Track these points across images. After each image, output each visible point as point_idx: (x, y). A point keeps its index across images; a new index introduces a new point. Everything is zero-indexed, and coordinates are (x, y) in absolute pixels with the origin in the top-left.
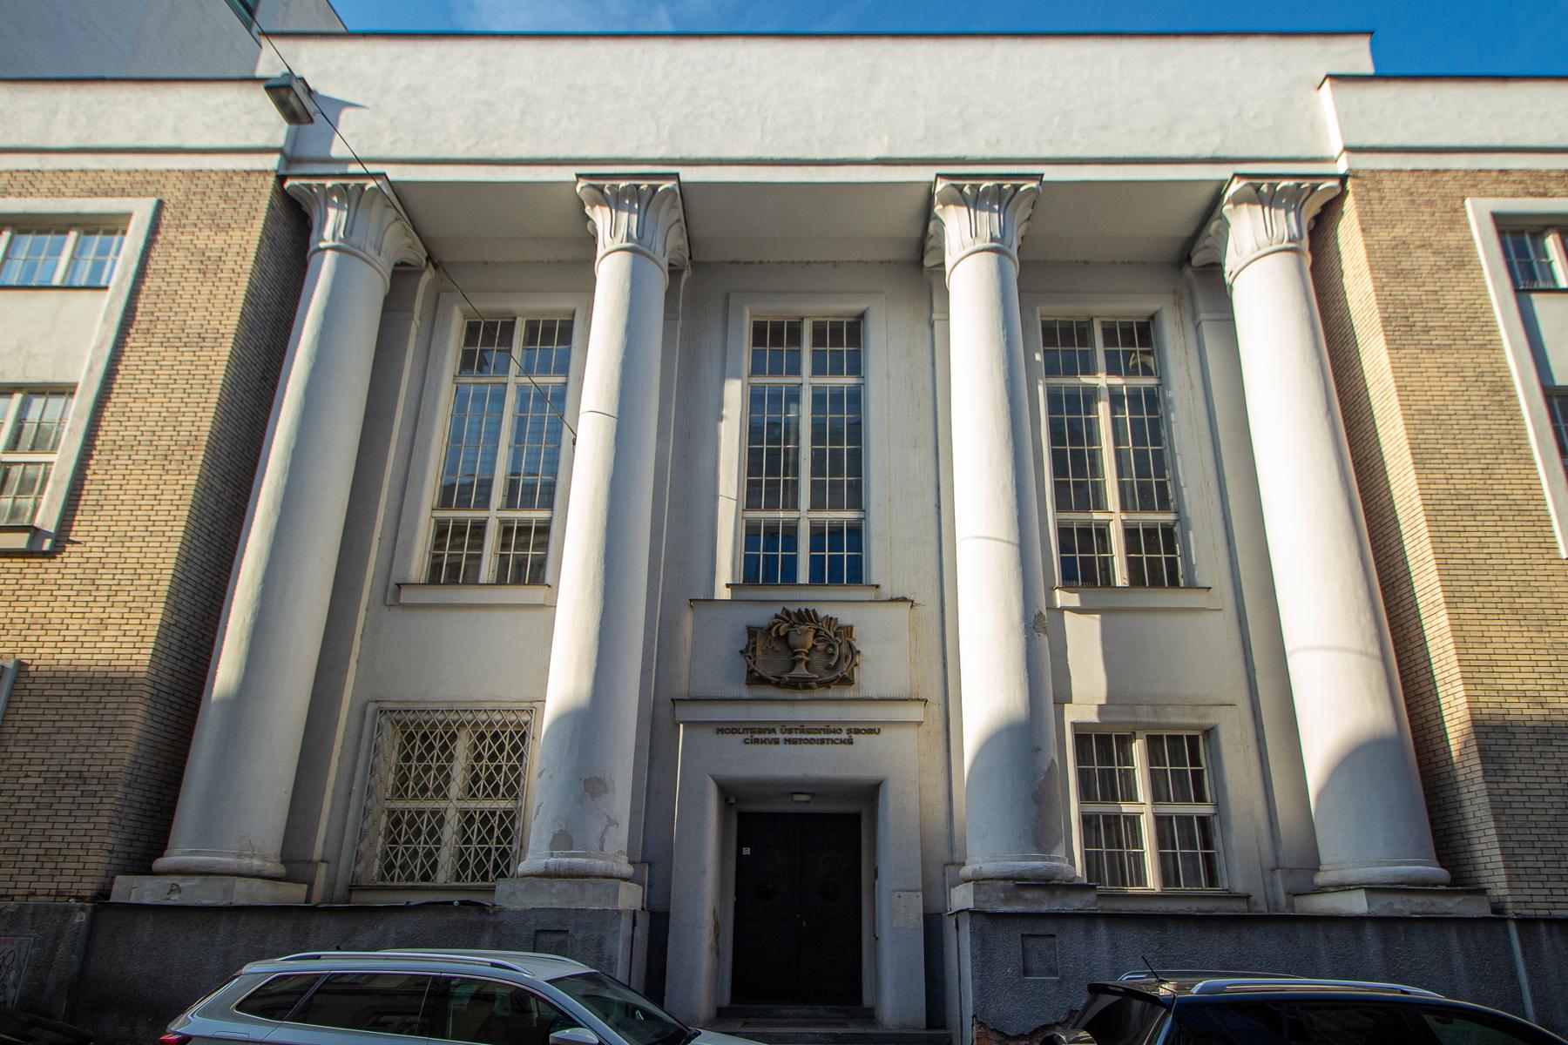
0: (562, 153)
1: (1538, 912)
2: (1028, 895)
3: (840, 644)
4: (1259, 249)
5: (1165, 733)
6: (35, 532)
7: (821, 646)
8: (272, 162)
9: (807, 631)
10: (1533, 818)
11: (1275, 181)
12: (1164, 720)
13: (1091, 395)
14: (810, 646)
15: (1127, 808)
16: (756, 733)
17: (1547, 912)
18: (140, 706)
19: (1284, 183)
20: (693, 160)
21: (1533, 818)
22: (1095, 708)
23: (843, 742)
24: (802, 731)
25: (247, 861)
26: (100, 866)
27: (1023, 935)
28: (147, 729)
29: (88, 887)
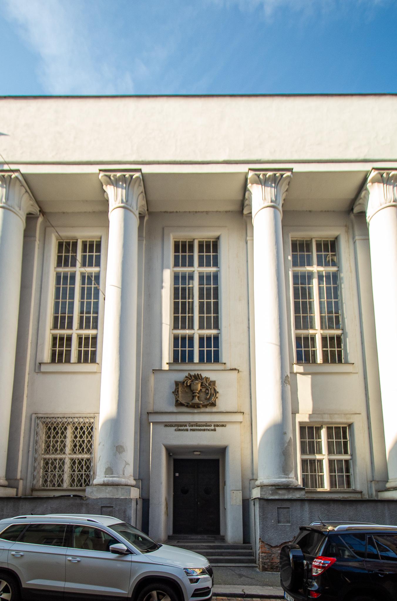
2: (280, 492)
3: (211, 389)
4: (381, 205)
9: (198, 383)
12: (333, 420)
13: (310, 276)
14: (199, 389)
16: (179, 426)
22: (308, 416)
23: (212, 430)
24: (197, 426)
27: (278, 508)
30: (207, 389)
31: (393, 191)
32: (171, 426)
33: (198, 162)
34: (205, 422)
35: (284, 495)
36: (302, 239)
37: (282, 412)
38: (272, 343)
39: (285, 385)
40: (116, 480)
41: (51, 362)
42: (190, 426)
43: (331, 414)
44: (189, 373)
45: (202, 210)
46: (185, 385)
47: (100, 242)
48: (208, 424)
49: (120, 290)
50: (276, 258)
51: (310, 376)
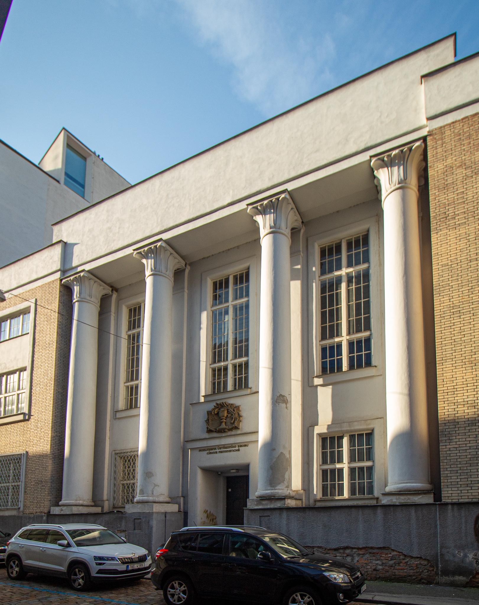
0: (126, 244)
1: (453, 501)
2: (264, 502)
3: (235, 414)
4: (387, 191)
5: (364, 432)
6: (24, 414)
7: (229, 415)
8: (58, 275)
9: (224, 411)
10: (459, 460)
11: (390, 153)
12: (352, 428)
13: (339, 280)
14: (226, 415)
15: (338, 466)
16: (211, 450)
17: (457, 500)
18: (50, 461)
19: (394, 153)
20: (168, 229)
21: (459, 460)
22: (326, 427)
23: (236, 450)
24: (224, 448)
25: (78, 501)
26: (48, 505)
27: (260, 516)
28: (54, 467)
29: (46, 511)
30: (232, 415)
31: (399, 171)
32: (204, 450)
33: (207, 213)
34: (230, 444)
35: (267, 505)
36: (331, 244)
37: (271, 431)
38: (263, 367)
39: (277, 404)
40: (145, 498)
41: (349, 370)
42: (218, 449)
43: (350, 423)
44: (216, 403)
45: (234, 247)
46: (213, 414)
47: (141, 306)
48: (226, 446)
49: (149, 346)
50: (273, 283)
51: (331, 387)
